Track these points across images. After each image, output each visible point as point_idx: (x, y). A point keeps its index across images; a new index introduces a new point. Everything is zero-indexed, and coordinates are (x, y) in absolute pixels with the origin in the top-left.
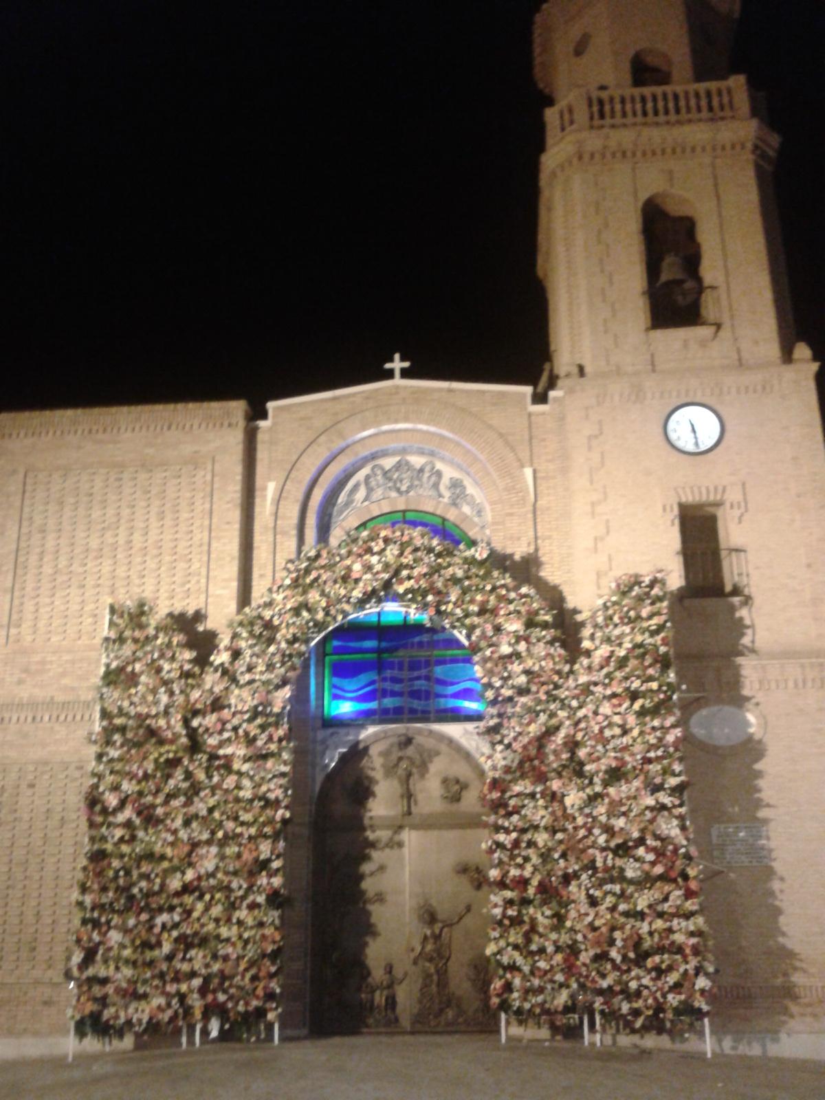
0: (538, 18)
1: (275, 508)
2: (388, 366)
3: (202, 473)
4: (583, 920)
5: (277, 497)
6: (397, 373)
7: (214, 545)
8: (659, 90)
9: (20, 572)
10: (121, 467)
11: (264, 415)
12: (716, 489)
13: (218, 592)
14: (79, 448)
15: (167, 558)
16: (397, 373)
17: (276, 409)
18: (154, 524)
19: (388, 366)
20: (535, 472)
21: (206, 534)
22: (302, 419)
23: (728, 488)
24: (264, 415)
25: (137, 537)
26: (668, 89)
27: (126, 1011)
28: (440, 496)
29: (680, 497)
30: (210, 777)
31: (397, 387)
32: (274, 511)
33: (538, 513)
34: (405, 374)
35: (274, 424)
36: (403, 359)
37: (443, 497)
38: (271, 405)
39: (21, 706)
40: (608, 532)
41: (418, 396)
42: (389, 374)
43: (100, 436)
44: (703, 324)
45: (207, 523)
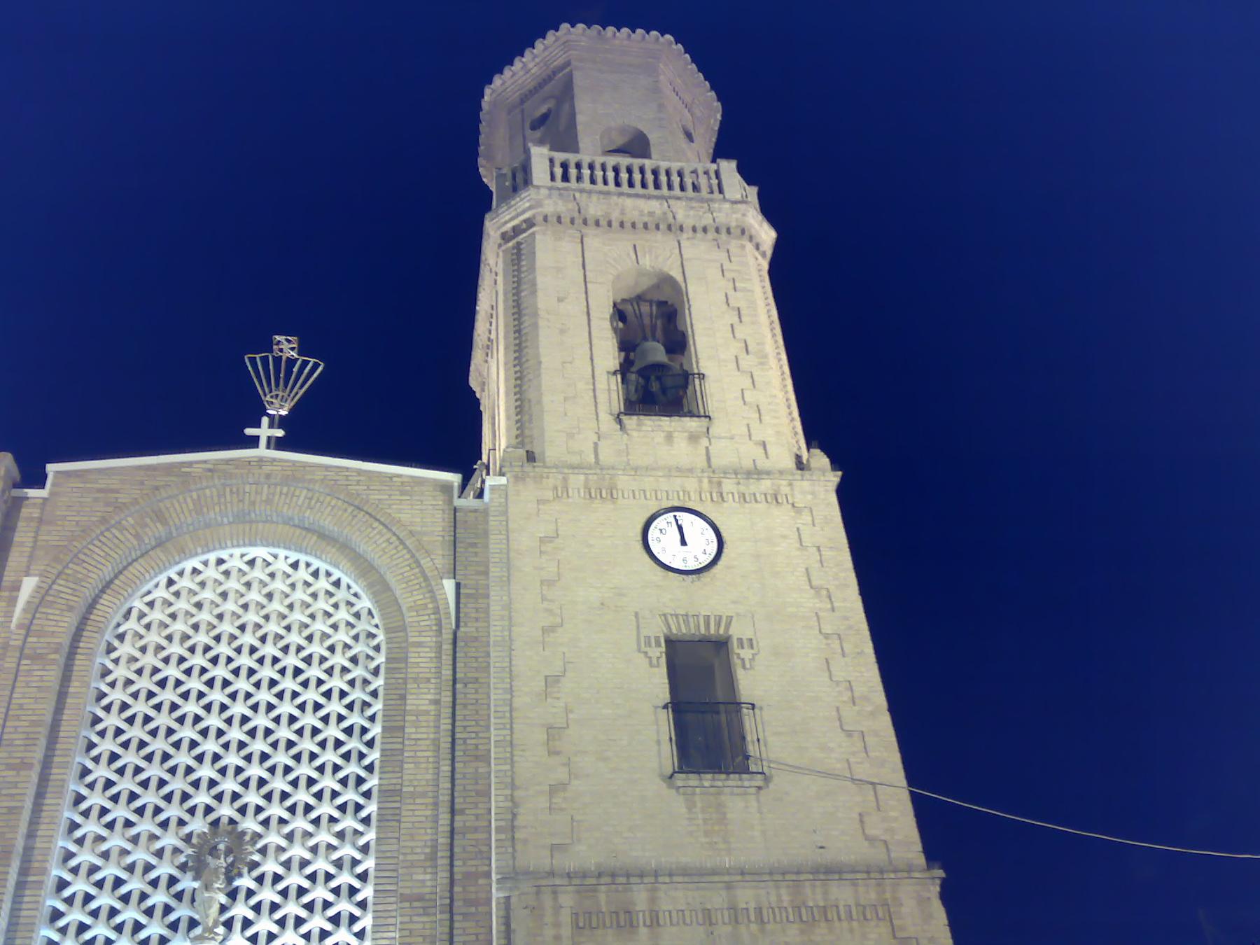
2: (249, 431)
4: (255, 843)
6: (263, 442)
8: (636, 162)
11: (40, 481)
12: (707, 618)
19: (249, 431)
20: (458, 586)
22: (100, 491)
23: (734, 620)
24: (40, 481)
26: (648, 164)
29: (669, 627)
31: (261, 461)
33: (460, 644)
34: (279, 444)
35: (51, 494)
36: (258, 425)
40: (763, 773)
41: (294, 476)
42: (253, 442)
44: (691, 415)
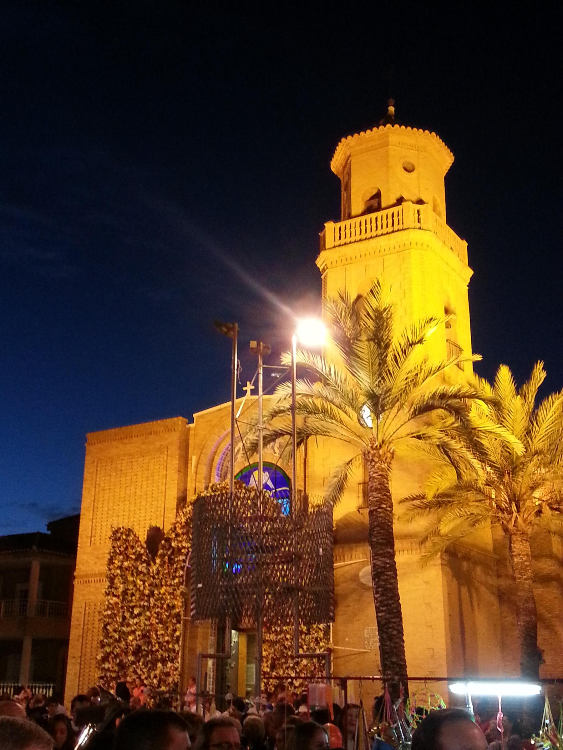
0: (453, 158)
1: (196, 469)
3: (163, 456)
5: (197, 464)
7: (168, 491)
9: (95, 510)
10: (131, 455)
13: (169, 515)
14: (117, 447)
15: (150, 500)
16: (249, 392)
17: (199, 417)
18: (145, 483)
21: (164, 487)
25: (138, 490)
27: (264, 683)
28: (275, 453)
30: (155, 613)
32: (195, 471)
37: (276, 453)
38: (195, 415)
39: (95, 575)
43: (126, 441)
45: (164, 481)
